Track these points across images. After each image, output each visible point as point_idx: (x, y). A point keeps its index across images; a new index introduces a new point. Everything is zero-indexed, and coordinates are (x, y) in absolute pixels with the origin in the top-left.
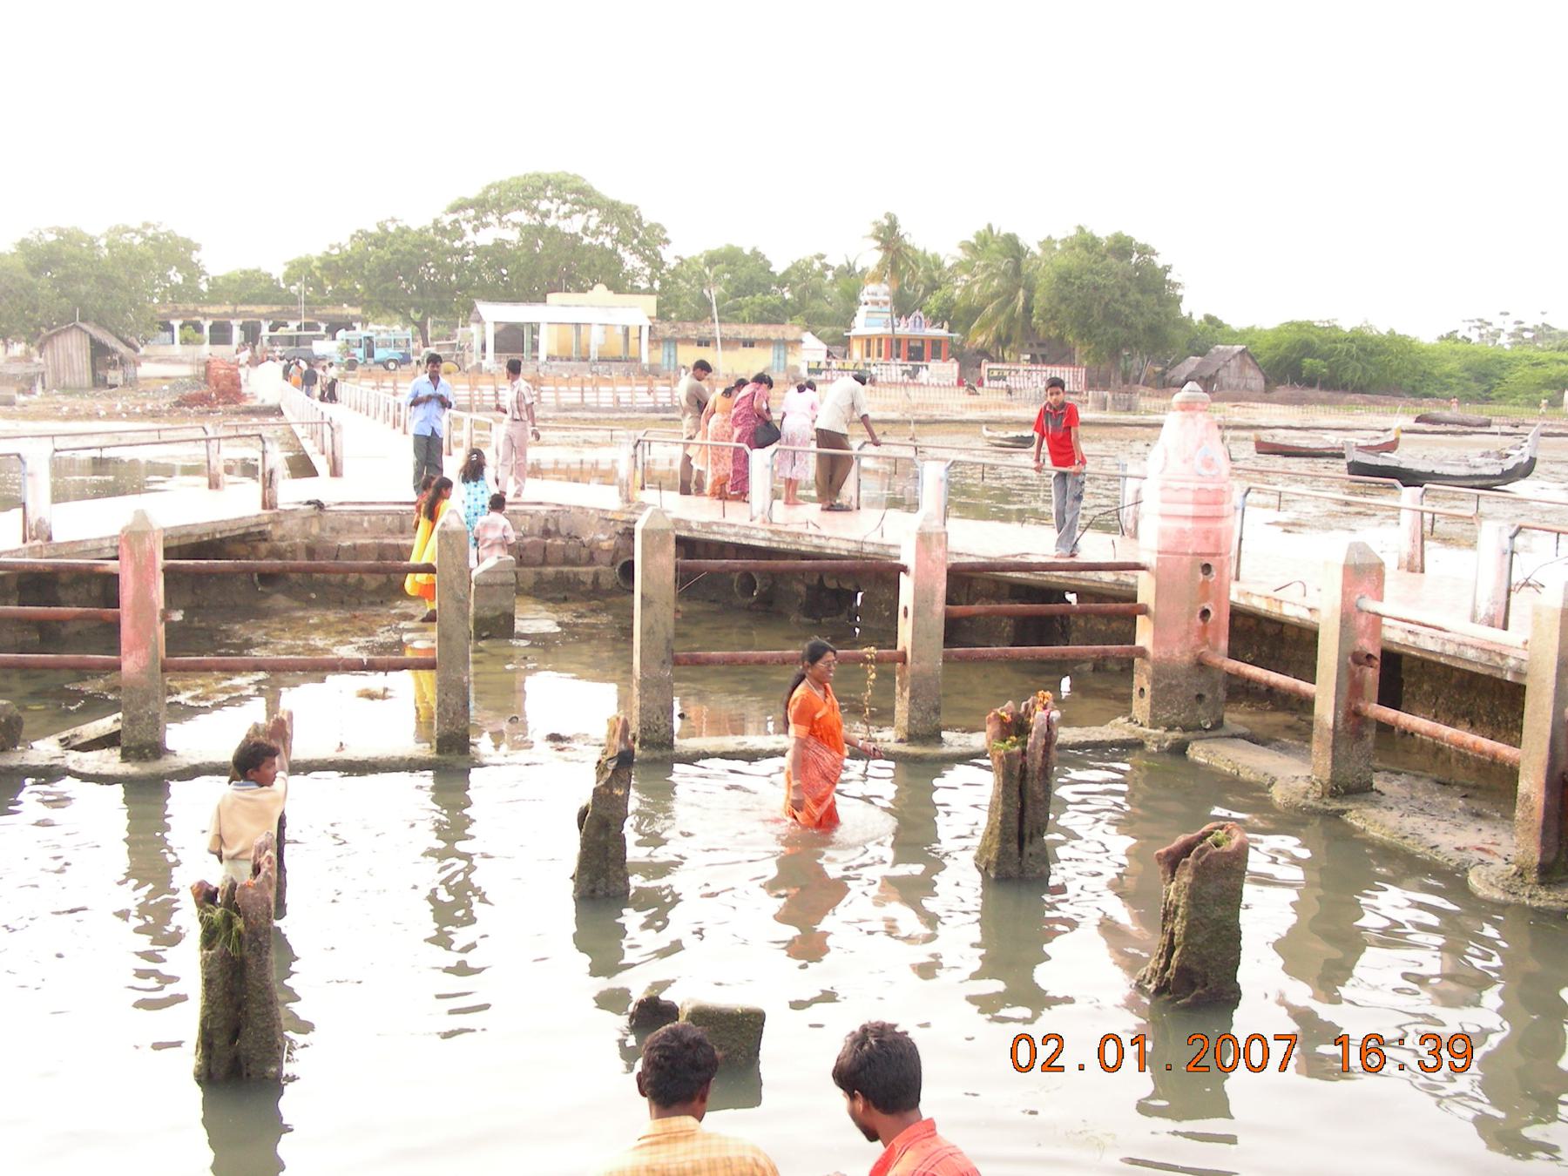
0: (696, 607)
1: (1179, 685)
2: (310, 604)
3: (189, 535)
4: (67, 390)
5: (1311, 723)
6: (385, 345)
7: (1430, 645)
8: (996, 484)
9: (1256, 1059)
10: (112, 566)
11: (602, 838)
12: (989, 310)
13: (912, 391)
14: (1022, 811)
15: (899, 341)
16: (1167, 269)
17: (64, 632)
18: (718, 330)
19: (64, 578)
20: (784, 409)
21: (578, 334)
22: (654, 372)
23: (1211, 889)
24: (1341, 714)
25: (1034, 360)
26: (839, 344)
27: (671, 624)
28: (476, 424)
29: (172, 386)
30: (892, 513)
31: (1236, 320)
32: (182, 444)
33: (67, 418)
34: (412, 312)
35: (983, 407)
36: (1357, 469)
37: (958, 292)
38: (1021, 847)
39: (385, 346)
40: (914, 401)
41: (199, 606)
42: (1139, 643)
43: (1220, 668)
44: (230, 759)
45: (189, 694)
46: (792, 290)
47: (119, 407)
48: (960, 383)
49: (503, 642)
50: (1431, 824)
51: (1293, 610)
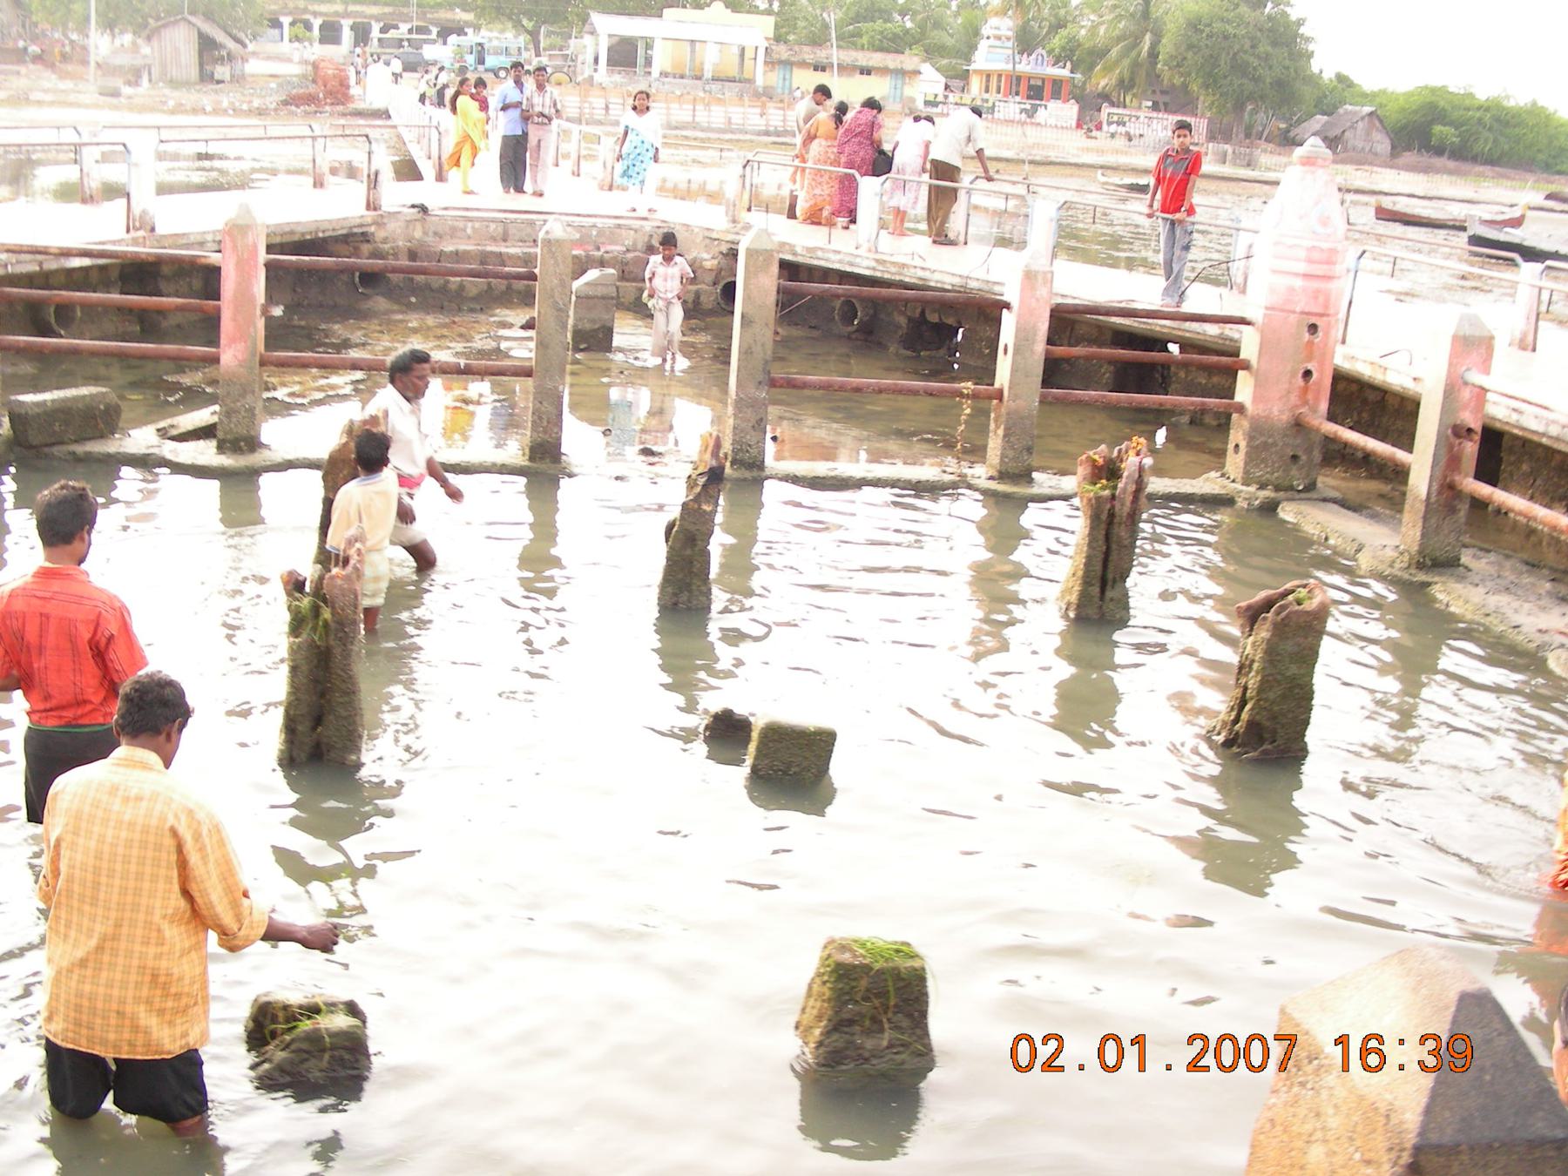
0: (796, 332)
1: (1275, 444)
2: (410, 307)
3: (292, 233)
4: (174, 84)
5: (1404, 494)
6: (497, 53)
7: (1534, 425)
8: (1107, 230)
9: (1256, 1059)
10: (215, 258)
11: (688, 552)
12: (1114, 52)
13: (1029, 130)
14: (1107, 554)
15: (1019, 78)
16: (1300, 22)
17: (165, 324)
18: (835, 55)
19: (165, 270)
20: (897, 138)
21: (693, 51)
22: (768, 94)
23: (1288, 646)
24: (1435, 487)
25: (1155, 107)
26: (958, 78)
27: (769, 345)
28: (585, 137)
29: (280, 85)
30: (1001, 252)
31: (1367, 81)
32: (294, 141)
33: (172, 112)
34: (525, 22)
35: (1100, 152)
36: (1476, 240)
37: (1083, 32)
38: (1103, 591)
39: (496, 53)
40: (1030, 141)
41: (299, 305)
42: (1239, 398)
43: (1318, 430)
44: (326, 457)
45: (286, 390)
46: (912, 20)
47: (225, 104)
48: (1079, 126)
49: (600, 355)
50: (1516, 604)
51: (1396, 377)
